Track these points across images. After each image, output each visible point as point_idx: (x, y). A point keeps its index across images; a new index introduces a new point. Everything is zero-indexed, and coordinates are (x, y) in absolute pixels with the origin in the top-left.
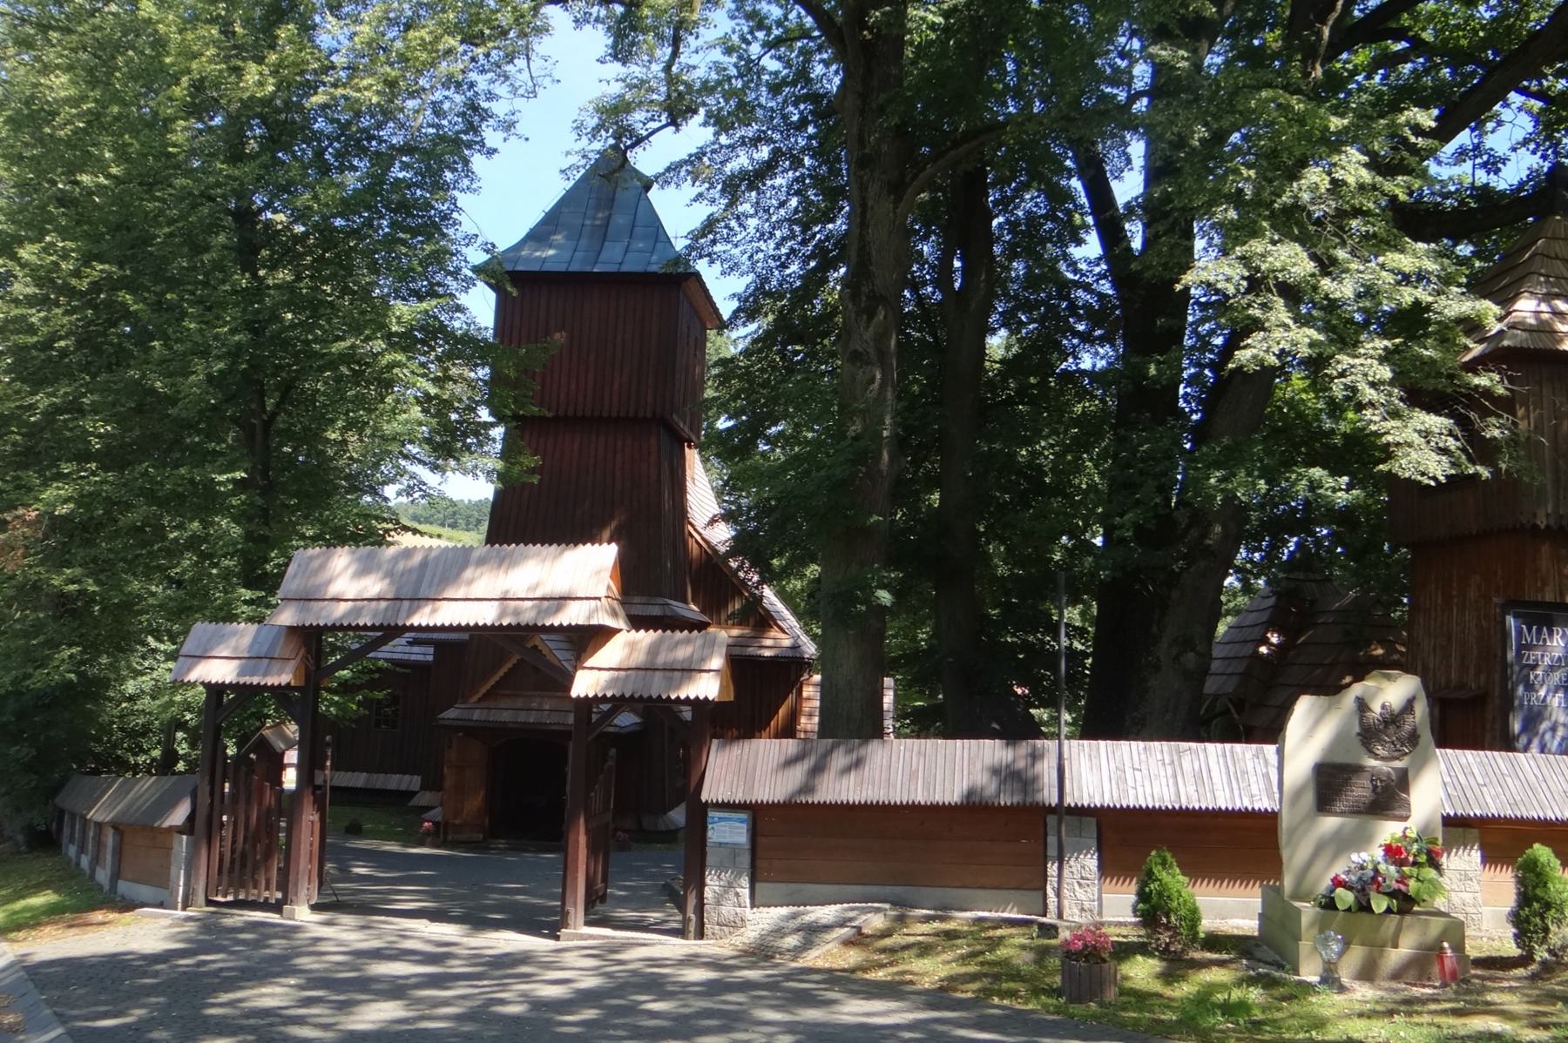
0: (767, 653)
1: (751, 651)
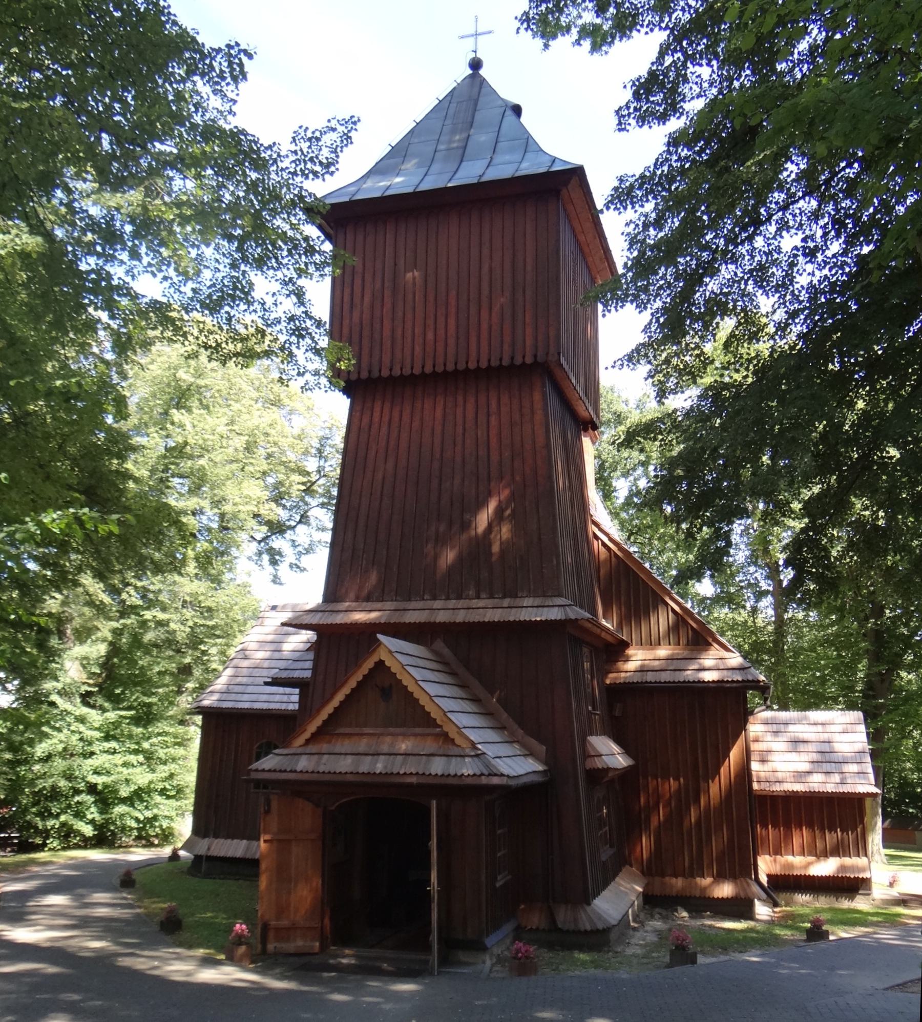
0: (709, 676)
1: (689, 675)
